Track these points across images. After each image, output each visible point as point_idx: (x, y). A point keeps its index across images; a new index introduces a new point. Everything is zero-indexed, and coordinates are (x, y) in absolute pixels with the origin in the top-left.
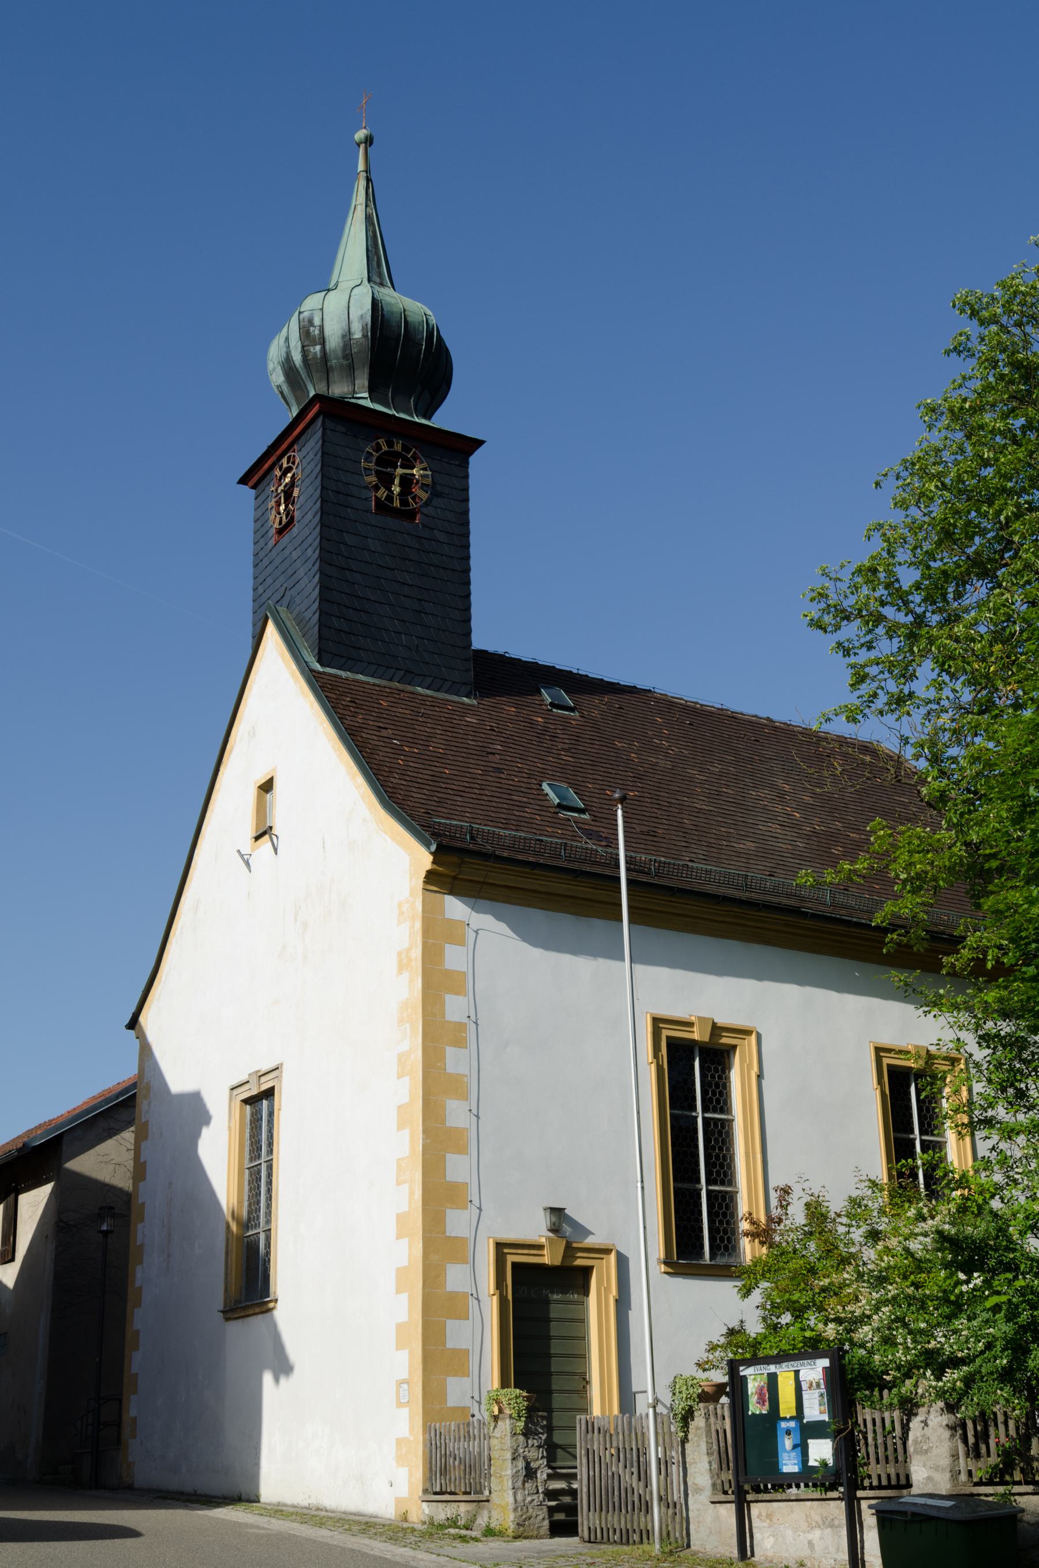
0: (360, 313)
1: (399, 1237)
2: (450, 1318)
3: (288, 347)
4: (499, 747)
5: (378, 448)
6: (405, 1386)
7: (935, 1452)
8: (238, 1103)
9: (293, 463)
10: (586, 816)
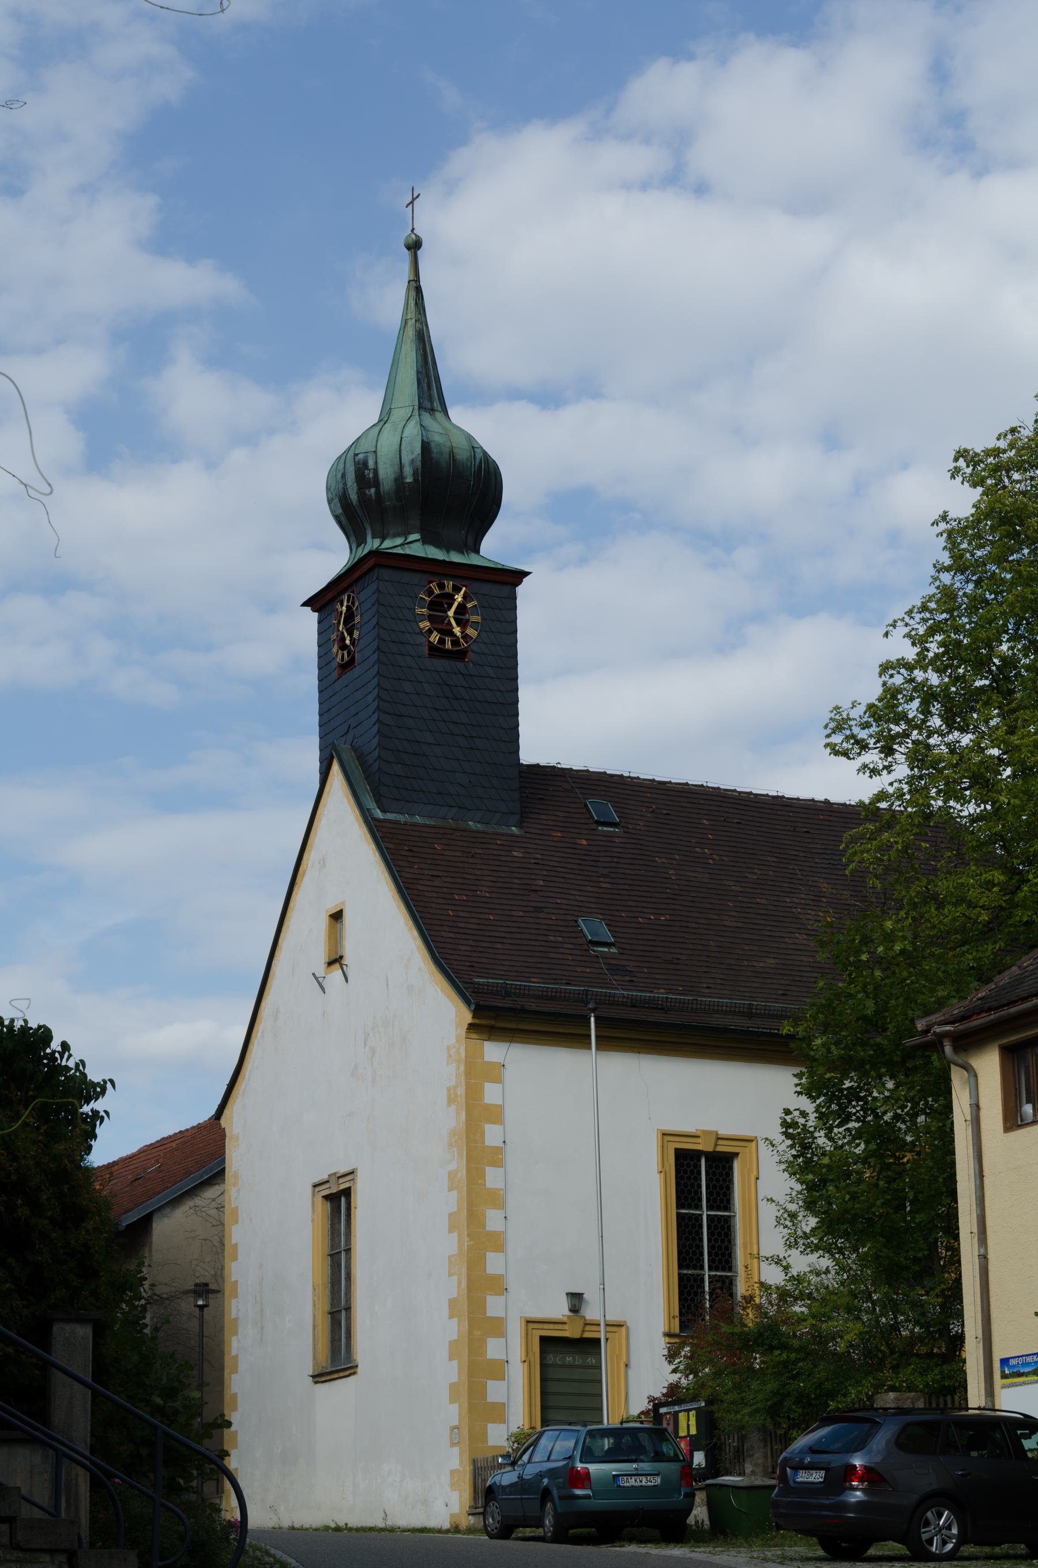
0: (411, 457)
3: (345, 484)
4: (541, 883)
5: (430, 592)
6: (456, 1431)
7: (756, 1455)
8: (320, 1199)
10: (613, 950)
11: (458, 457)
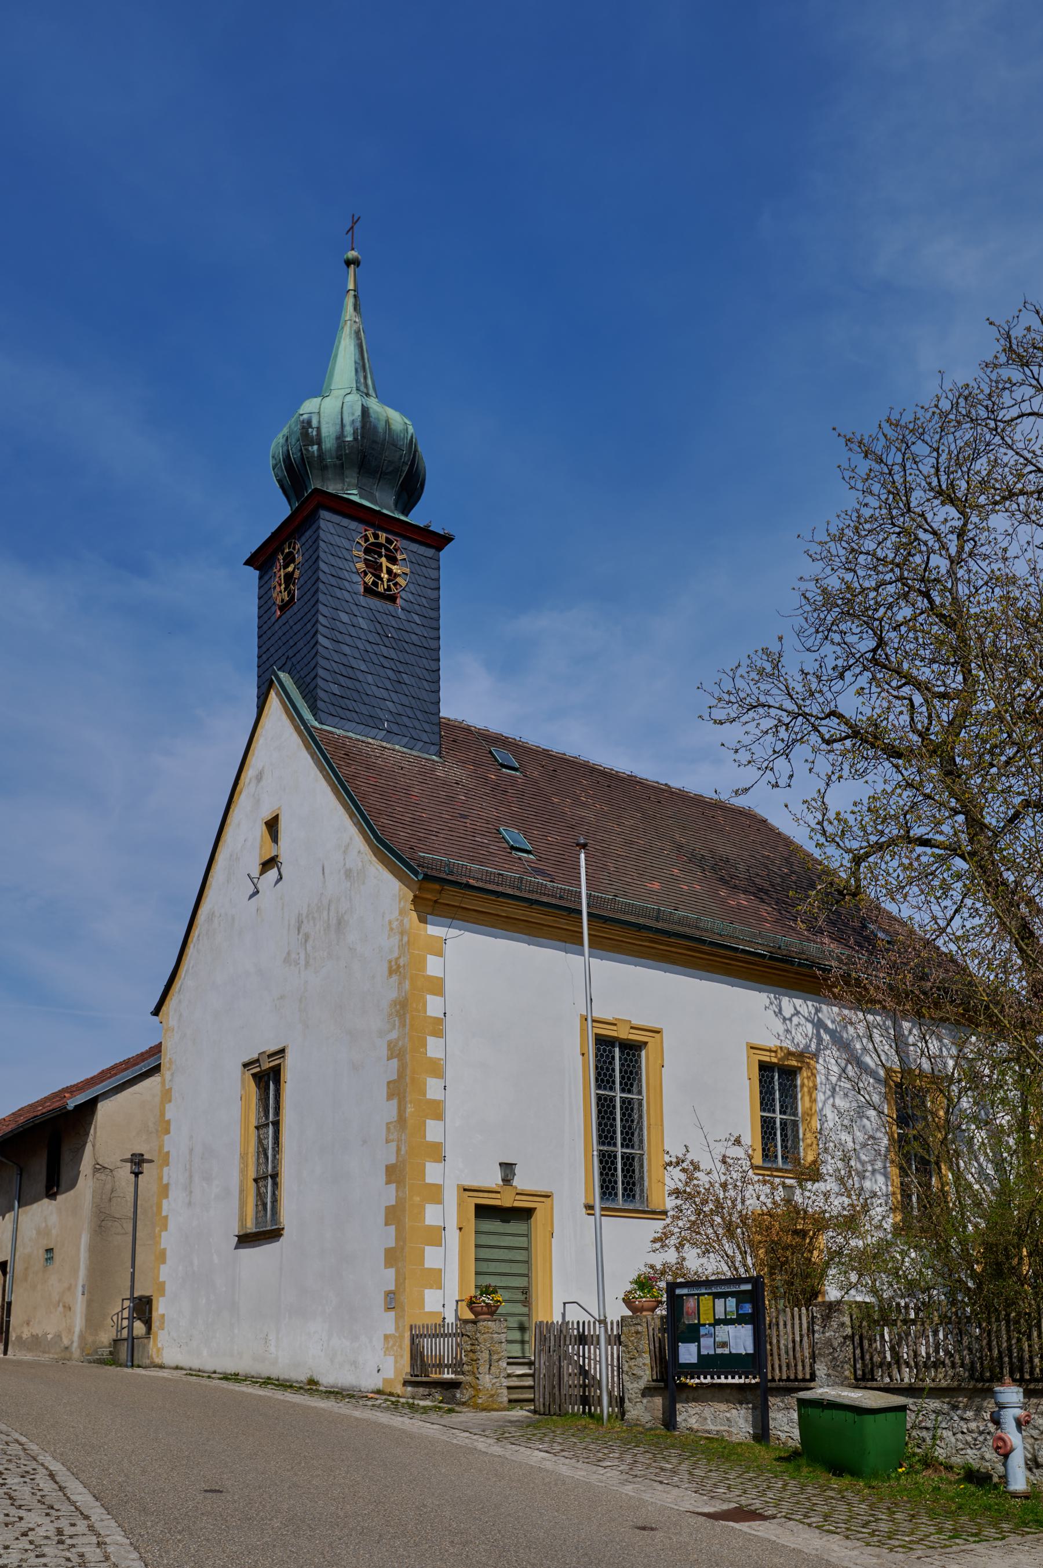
0: (351, 418)
1: (388, 1183)
2: (428, 1245)
6: (392, 1296)
9: (294, 548)
11: (393, 427)
